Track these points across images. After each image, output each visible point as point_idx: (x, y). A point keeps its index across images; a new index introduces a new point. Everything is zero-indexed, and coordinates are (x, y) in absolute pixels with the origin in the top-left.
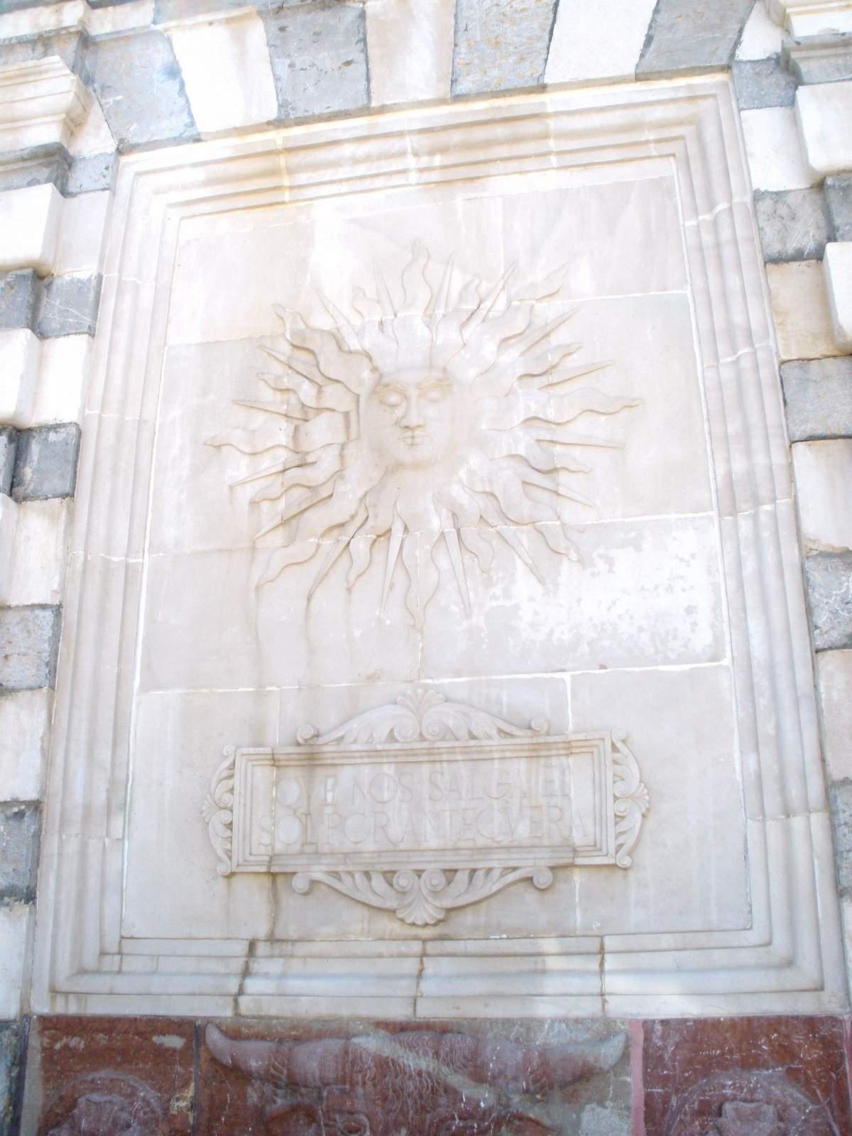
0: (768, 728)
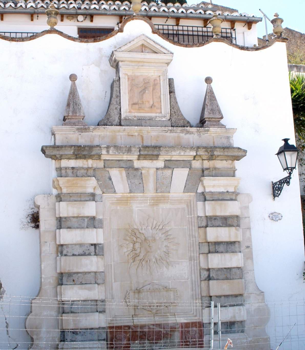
0: (194, 289)
